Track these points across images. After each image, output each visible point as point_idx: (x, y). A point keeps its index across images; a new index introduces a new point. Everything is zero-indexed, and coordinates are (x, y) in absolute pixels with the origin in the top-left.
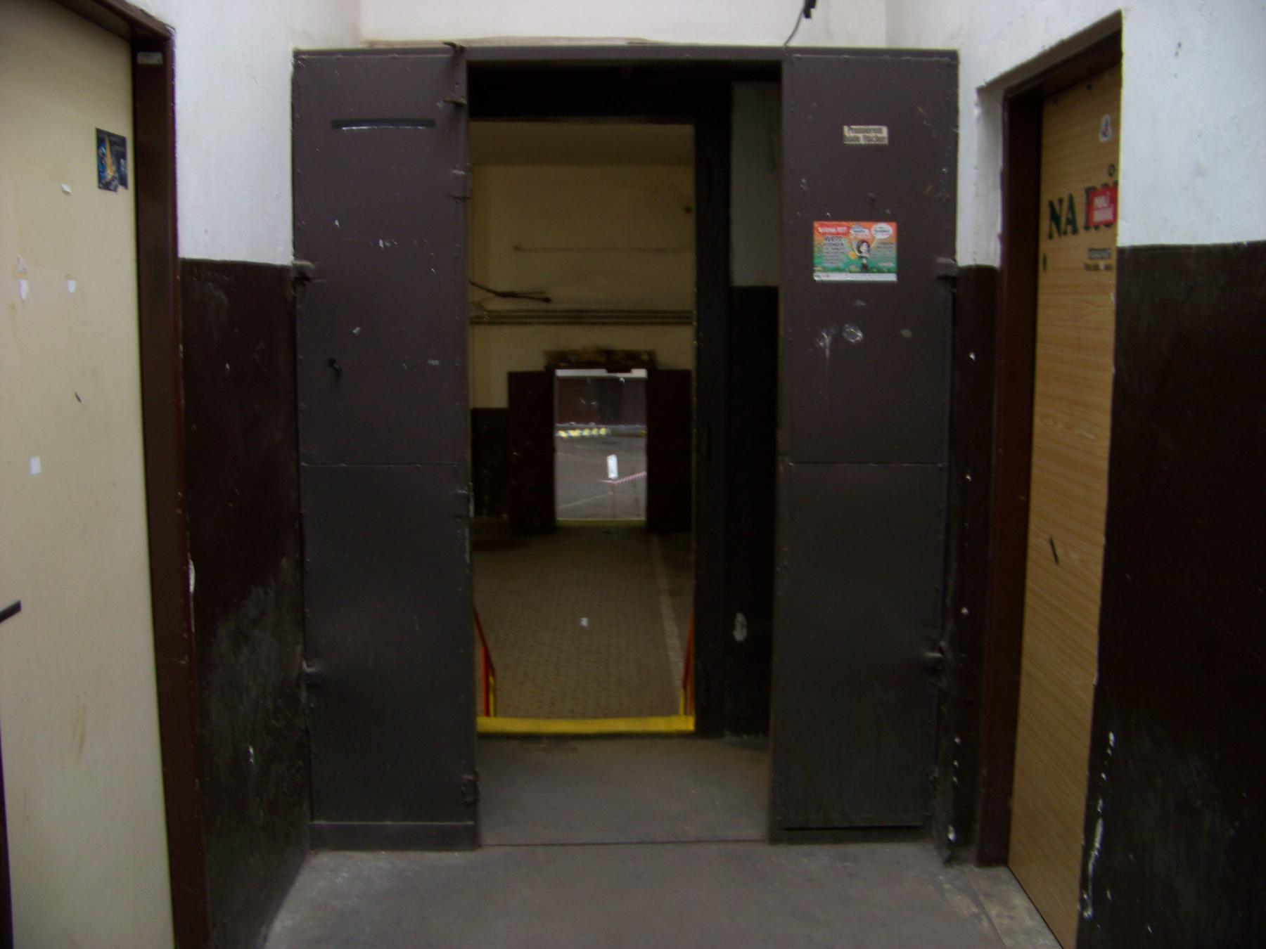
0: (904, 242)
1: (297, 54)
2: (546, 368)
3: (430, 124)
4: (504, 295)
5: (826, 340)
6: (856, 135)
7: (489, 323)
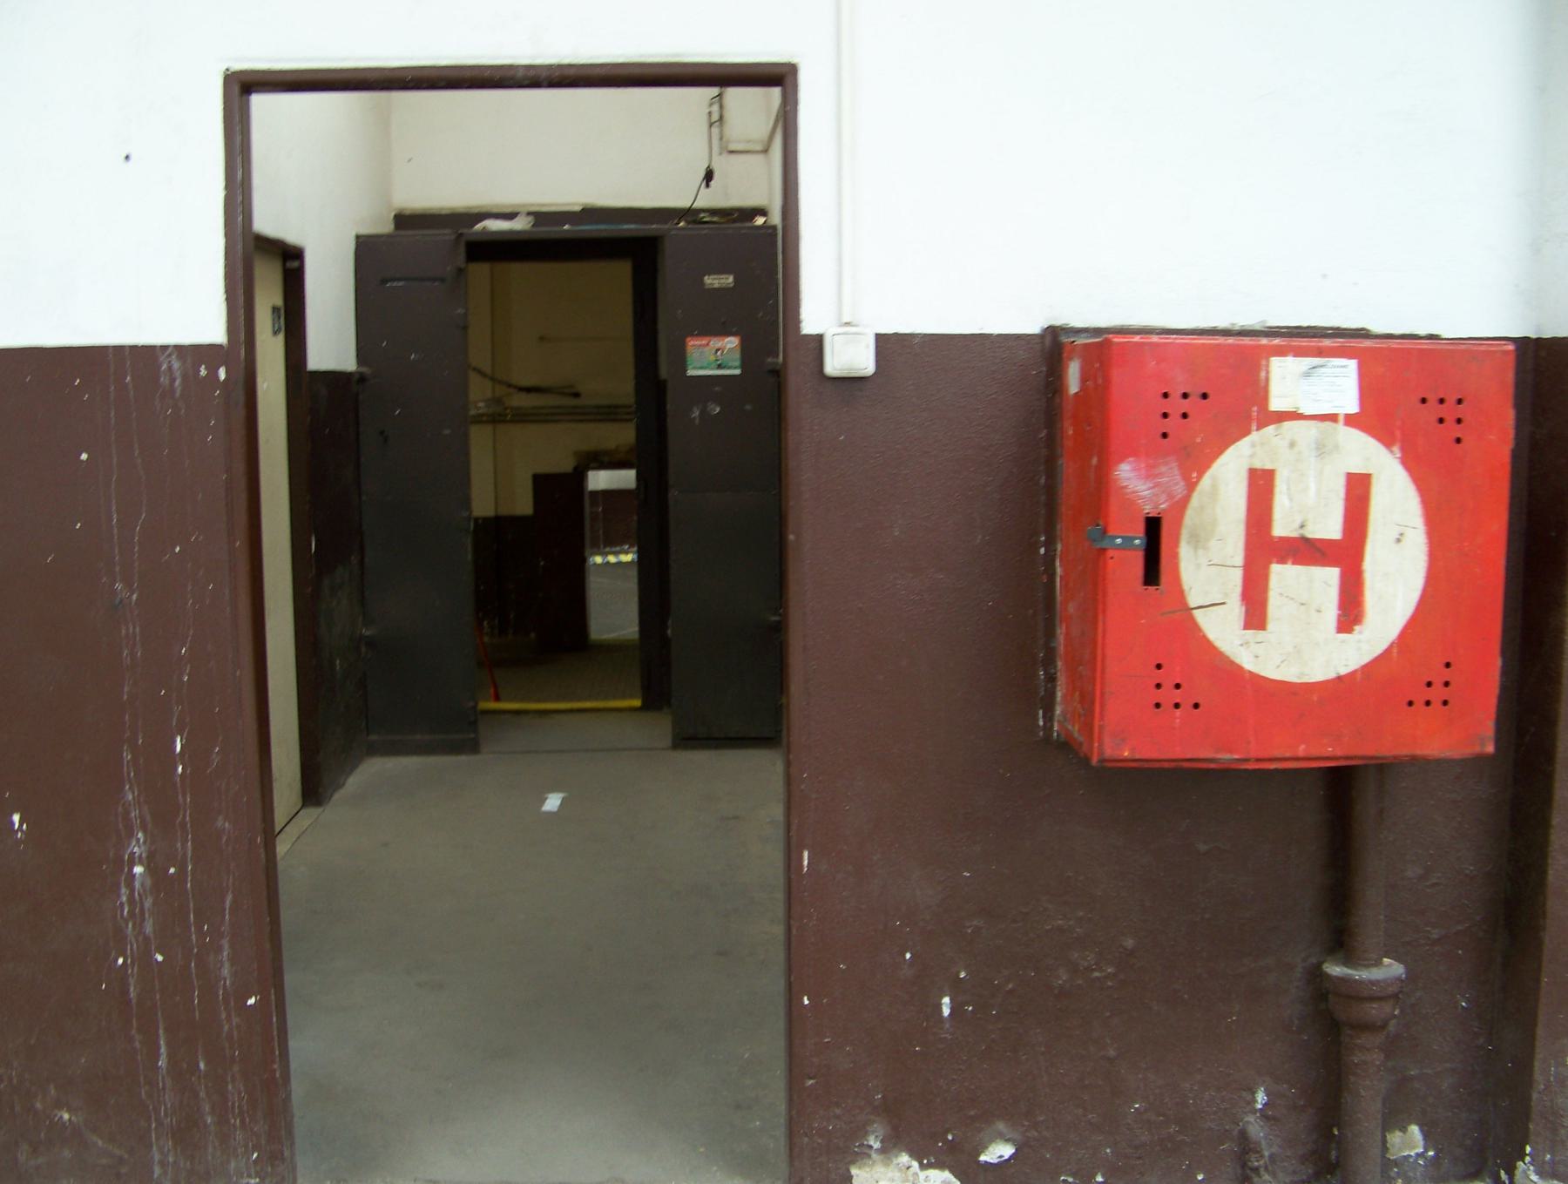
0: (745, 348)
1: (358, 237)
2: (575, 469)
3: (443, 280)
4: (528, 390)
5: (696, 413)
6: (712, 281)
7: (512, 421)
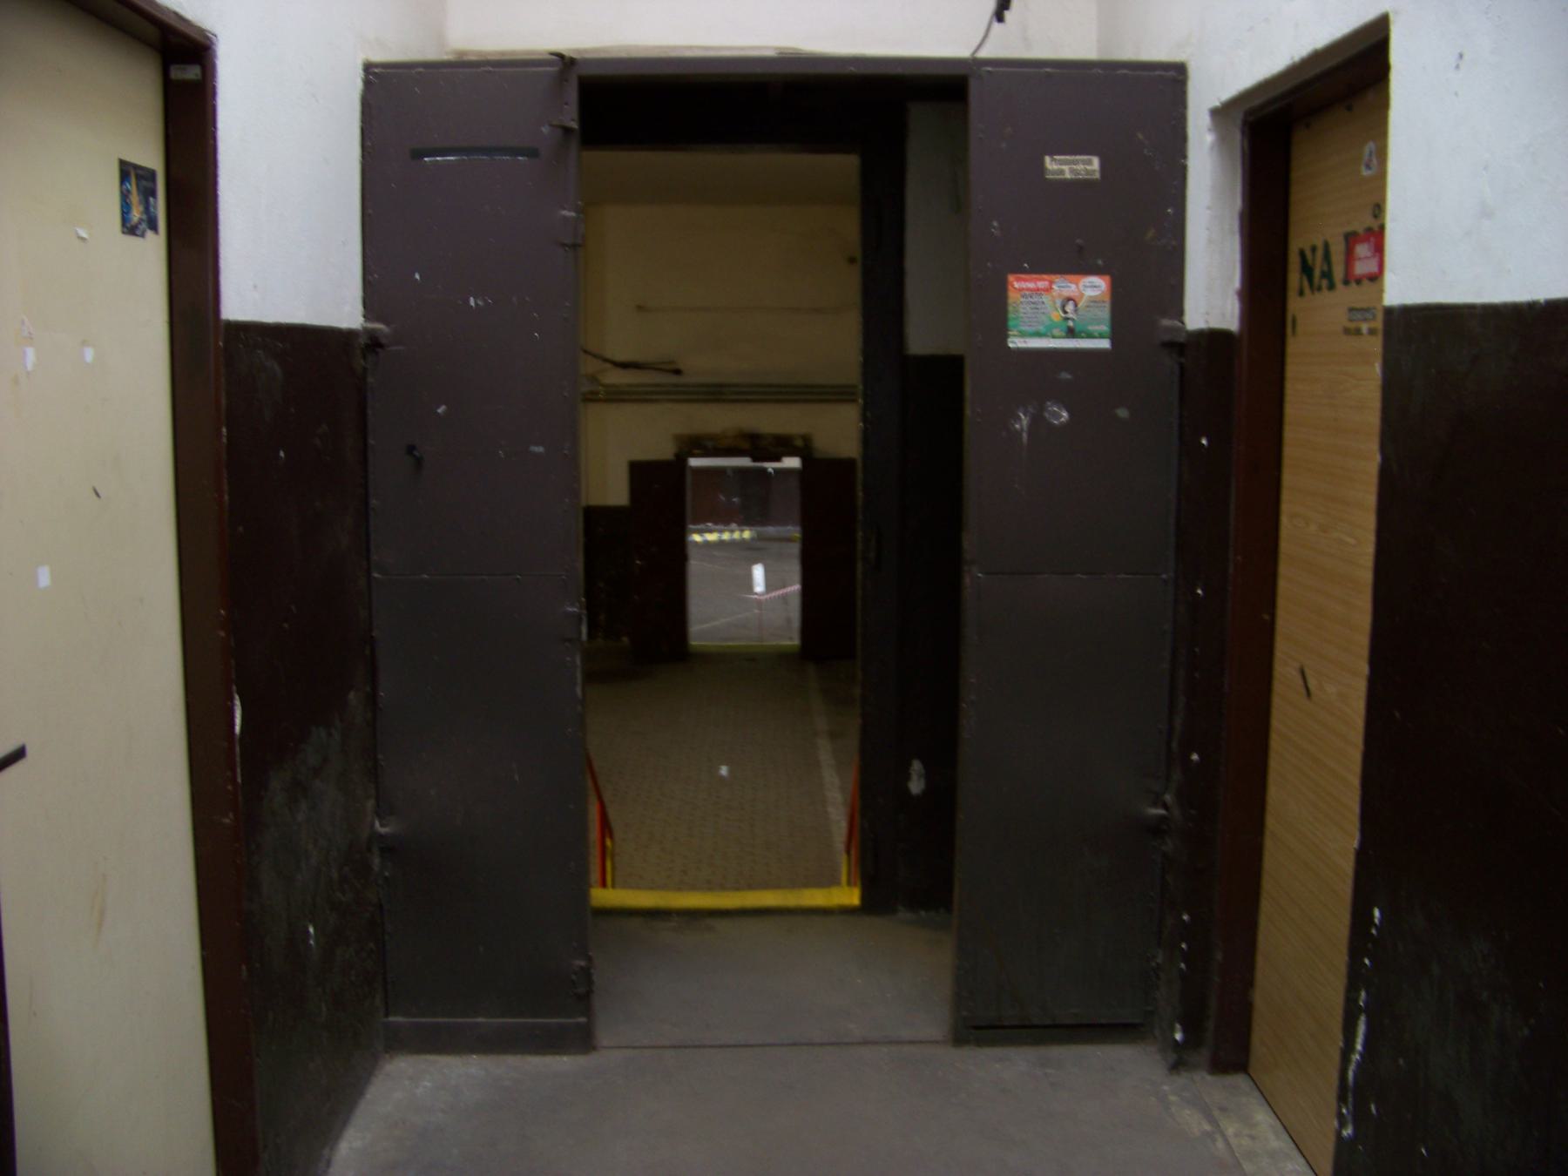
0: (1120, 300)
1: (368, 67)
2: (677, 455)
3: (532, 153)
4: (624, 366)
5: (1023, 421)
6: (1060, 167)
7: (606, 401)
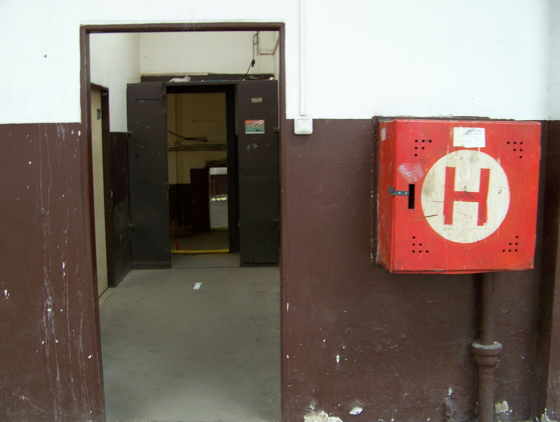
0: (266, 124)
1: (128, 85)
2: (206, 167)
3: (158, 100)
4: (189, 139)
5: (249, 147)
6: (254, 100)
7: (183, 150)
